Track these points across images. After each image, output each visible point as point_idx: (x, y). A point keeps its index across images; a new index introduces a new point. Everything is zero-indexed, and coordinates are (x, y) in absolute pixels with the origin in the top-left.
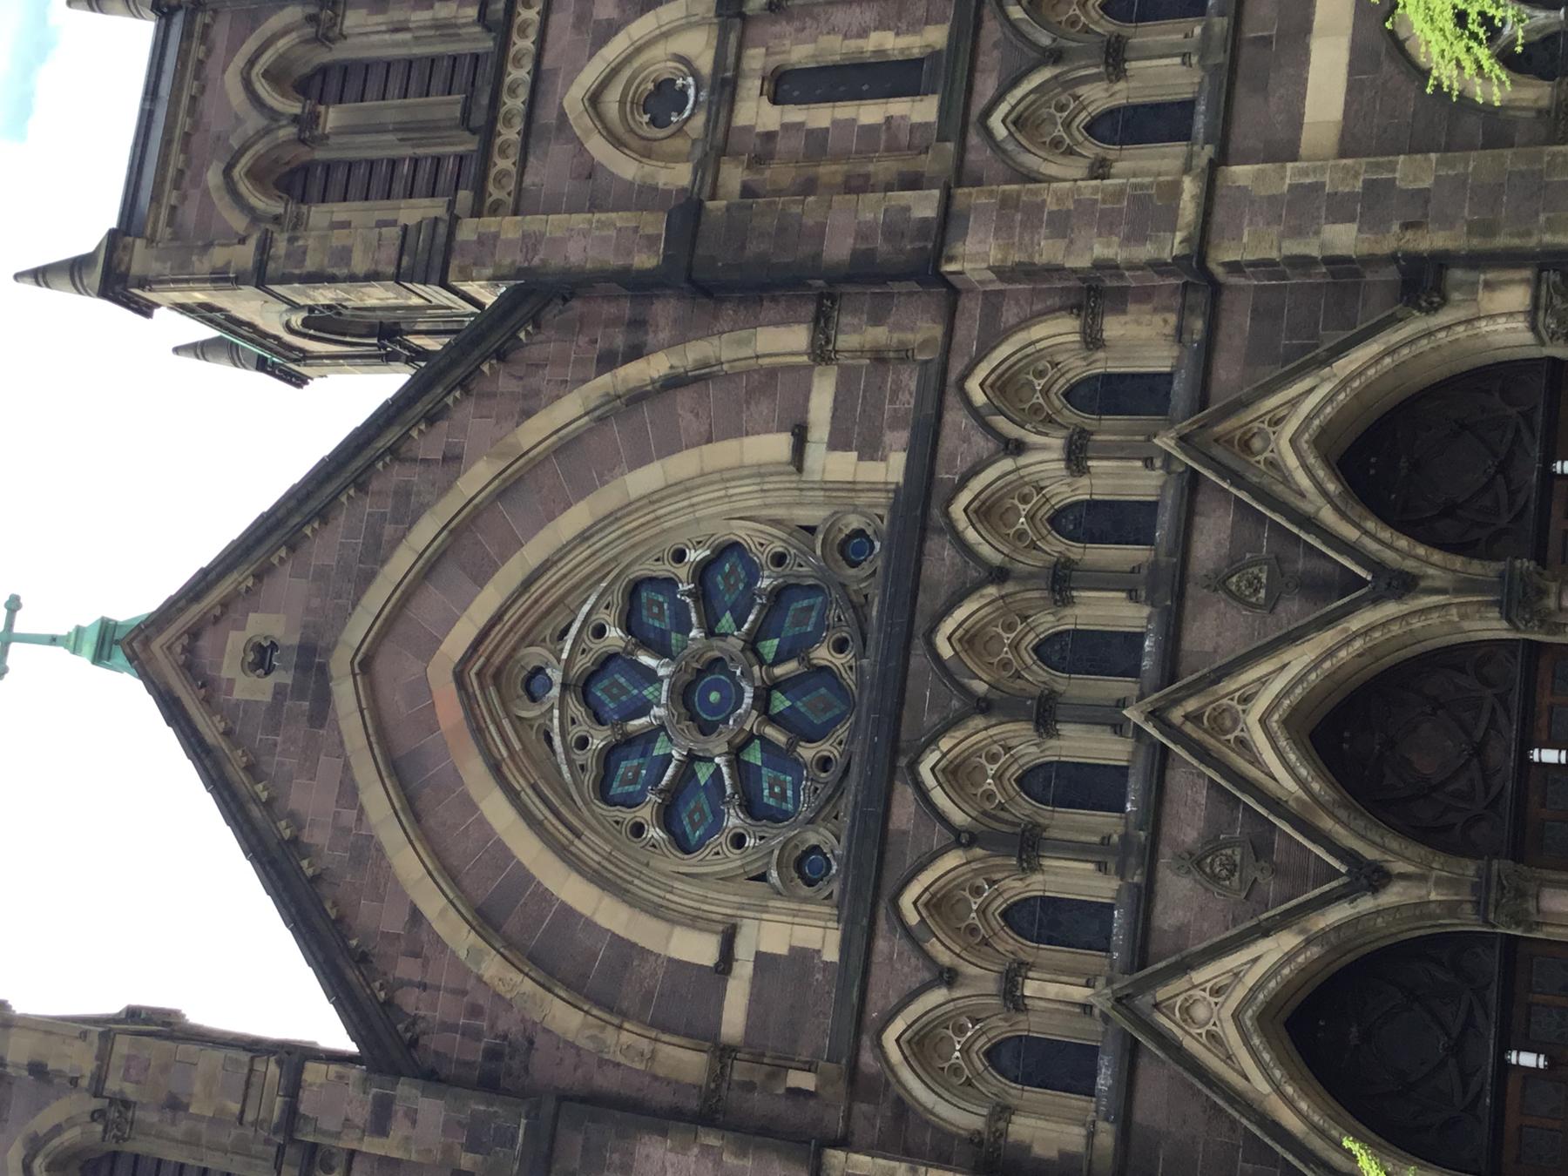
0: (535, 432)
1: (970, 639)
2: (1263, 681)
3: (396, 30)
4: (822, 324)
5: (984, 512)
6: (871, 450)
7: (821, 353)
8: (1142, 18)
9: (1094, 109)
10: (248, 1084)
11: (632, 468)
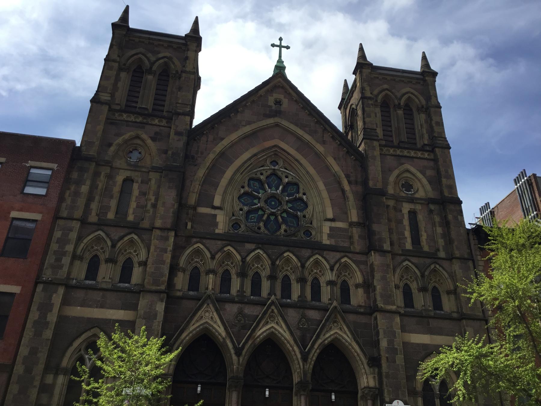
0: (331, 160)
1: (288, 260)
2: (281, 327)
3: (421, 125)
4: (358, 224)
5: (317, 263)
6: (330, 236)
7: (351, 224)
8: (433, 296)
9: (411, 285)
10: (185, 104)
11: (323, 183)
